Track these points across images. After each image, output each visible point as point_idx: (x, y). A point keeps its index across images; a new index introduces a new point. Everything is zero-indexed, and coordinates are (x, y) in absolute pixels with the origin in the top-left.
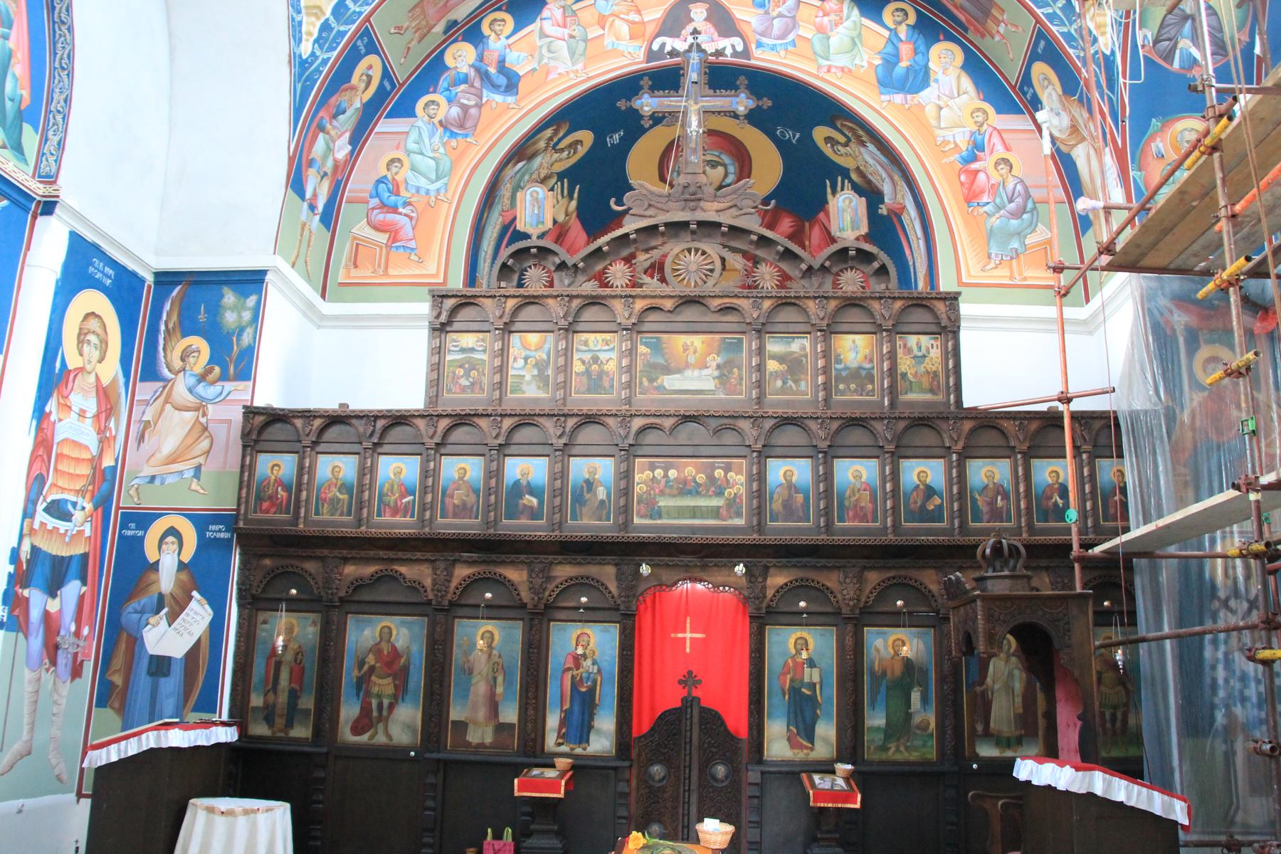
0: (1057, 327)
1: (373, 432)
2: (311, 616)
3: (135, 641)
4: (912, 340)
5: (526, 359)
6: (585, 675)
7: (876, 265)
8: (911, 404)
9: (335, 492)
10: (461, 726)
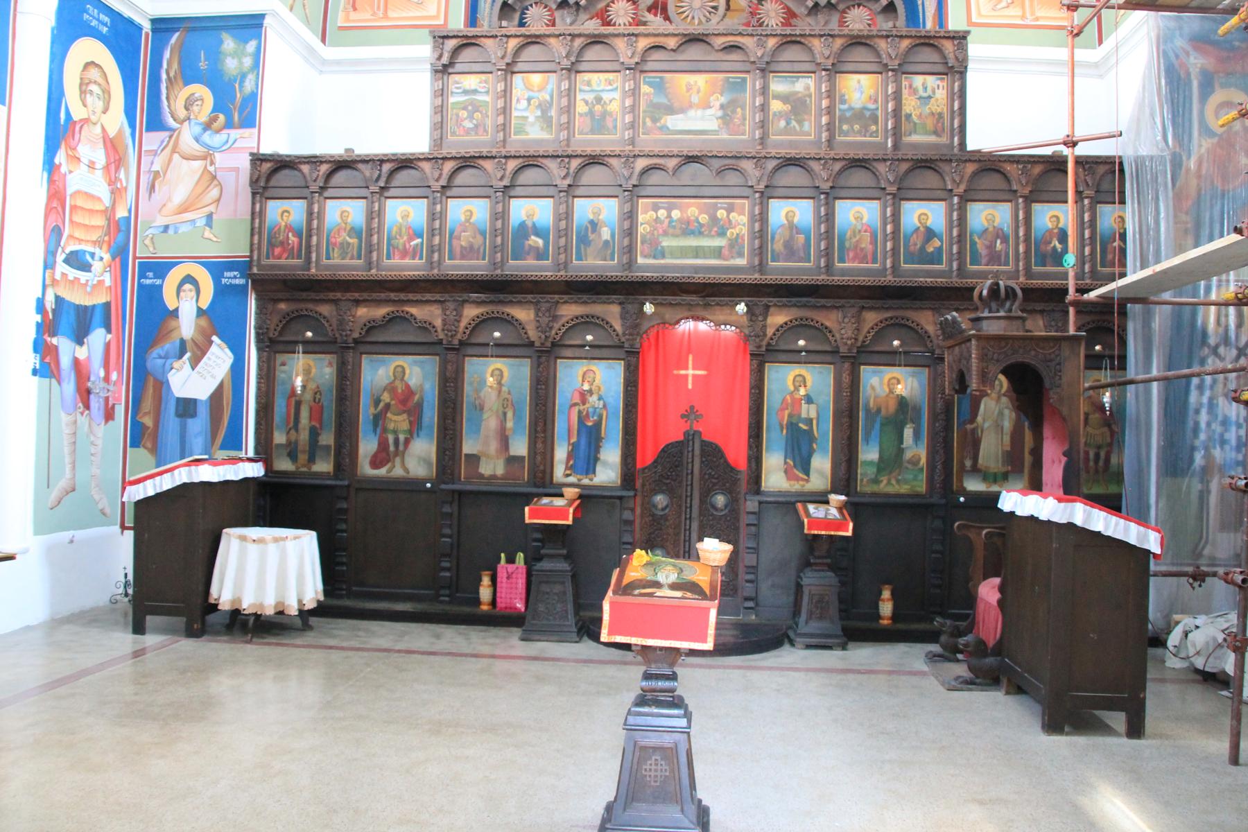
0: (1067, 70)
1: (379, 176)
2: (328, 357)
3: (161, 386)
4: (918, 80)
5: (529, 100)
6: (591, 410)
8: (914, 146)
9: (344, 237)
10: (474, 459)
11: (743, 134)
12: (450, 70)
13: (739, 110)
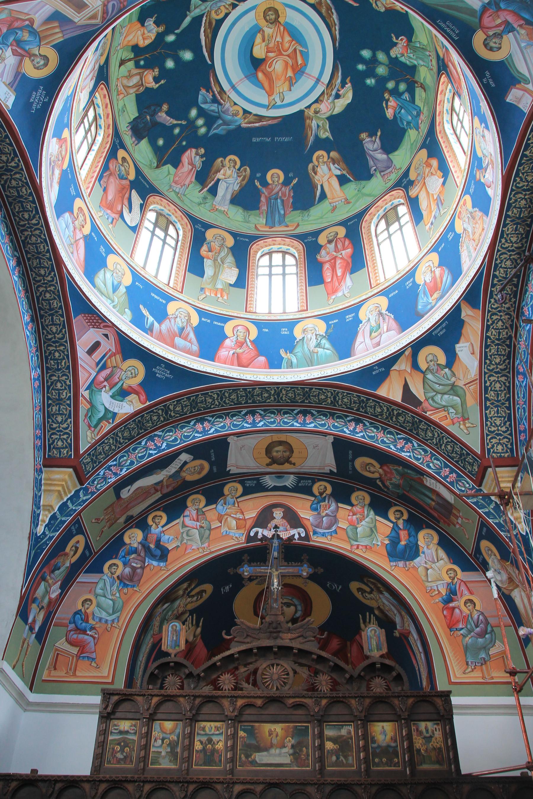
5: (163, 740)
7: (394, 674)
8: (426, 772)
11: (308, 766)
12: (112, 717)
13: (304, 749)
